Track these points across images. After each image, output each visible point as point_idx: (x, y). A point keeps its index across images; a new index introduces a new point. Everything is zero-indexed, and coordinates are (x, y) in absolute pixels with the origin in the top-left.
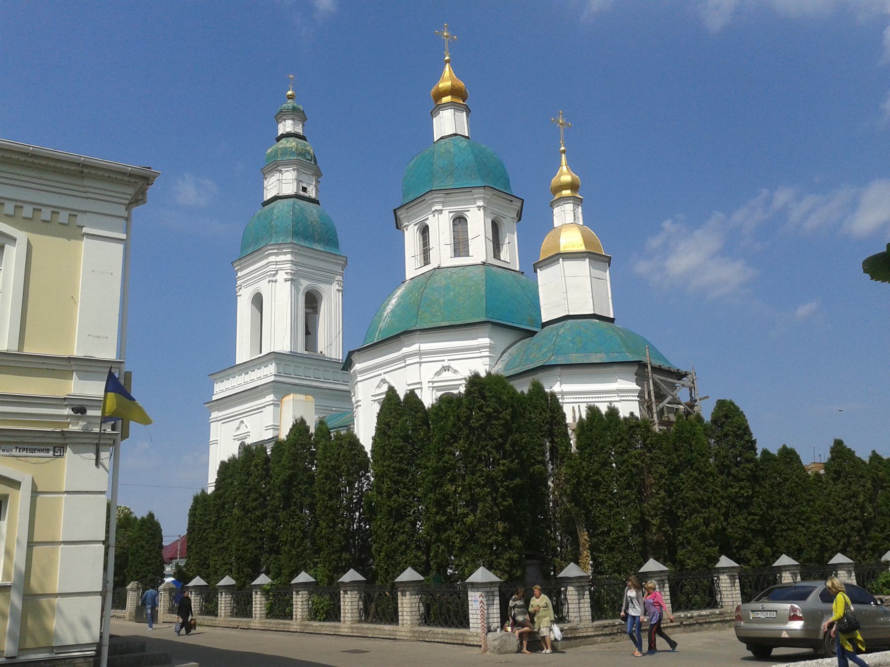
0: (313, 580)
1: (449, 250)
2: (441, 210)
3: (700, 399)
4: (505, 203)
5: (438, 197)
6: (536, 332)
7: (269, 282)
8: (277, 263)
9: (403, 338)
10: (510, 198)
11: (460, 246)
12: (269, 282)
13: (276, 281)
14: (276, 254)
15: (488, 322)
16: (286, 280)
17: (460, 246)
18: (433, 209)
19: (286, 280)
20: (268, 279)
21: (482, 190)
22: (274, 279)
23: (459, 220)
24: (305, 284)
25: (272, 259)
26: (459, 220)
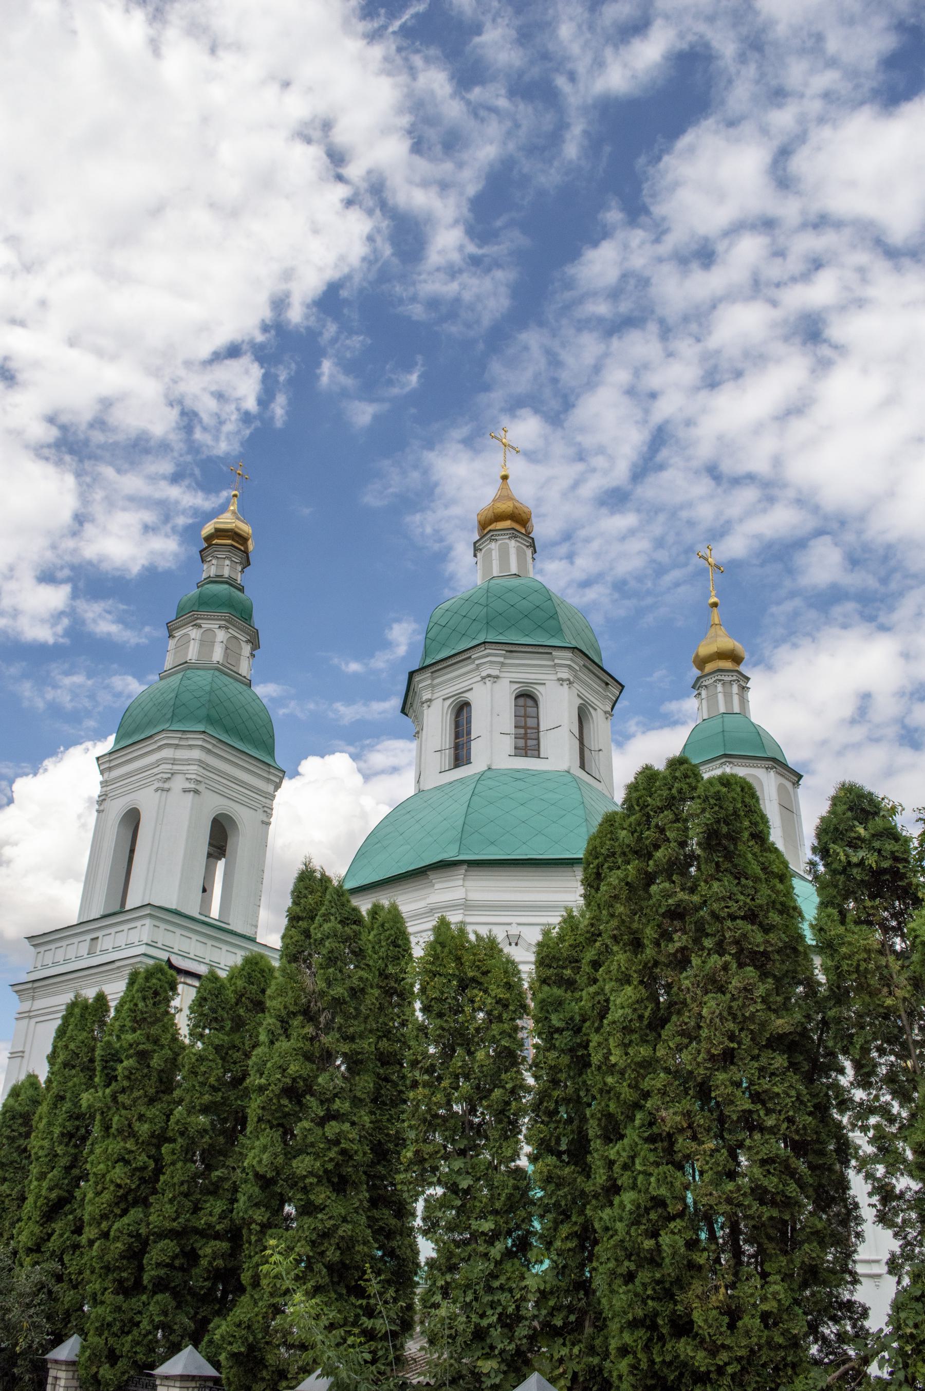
0: (211, 1371)
1: (508, 744)
2: (497, 677)
3: (877, 1261)
4: (597, 685)
5: (496, 656)
7: (157, 790)
8: (174, 761)
9: (432, 875)
10: (609, 680)
11: (528, 740)
12: (157, 790)
13: (168, 790)
14: (177, 746)
15: (725, 756)
16: (185, 791)
17: (528, 740)
18: (484, 674)
19: (185, 791)
20: (155, 787)
21: (569, 654)
22: (166, 786)
23: (526, 698)
24: (213, 804)
25: (167, 753)
26: (526, 698)
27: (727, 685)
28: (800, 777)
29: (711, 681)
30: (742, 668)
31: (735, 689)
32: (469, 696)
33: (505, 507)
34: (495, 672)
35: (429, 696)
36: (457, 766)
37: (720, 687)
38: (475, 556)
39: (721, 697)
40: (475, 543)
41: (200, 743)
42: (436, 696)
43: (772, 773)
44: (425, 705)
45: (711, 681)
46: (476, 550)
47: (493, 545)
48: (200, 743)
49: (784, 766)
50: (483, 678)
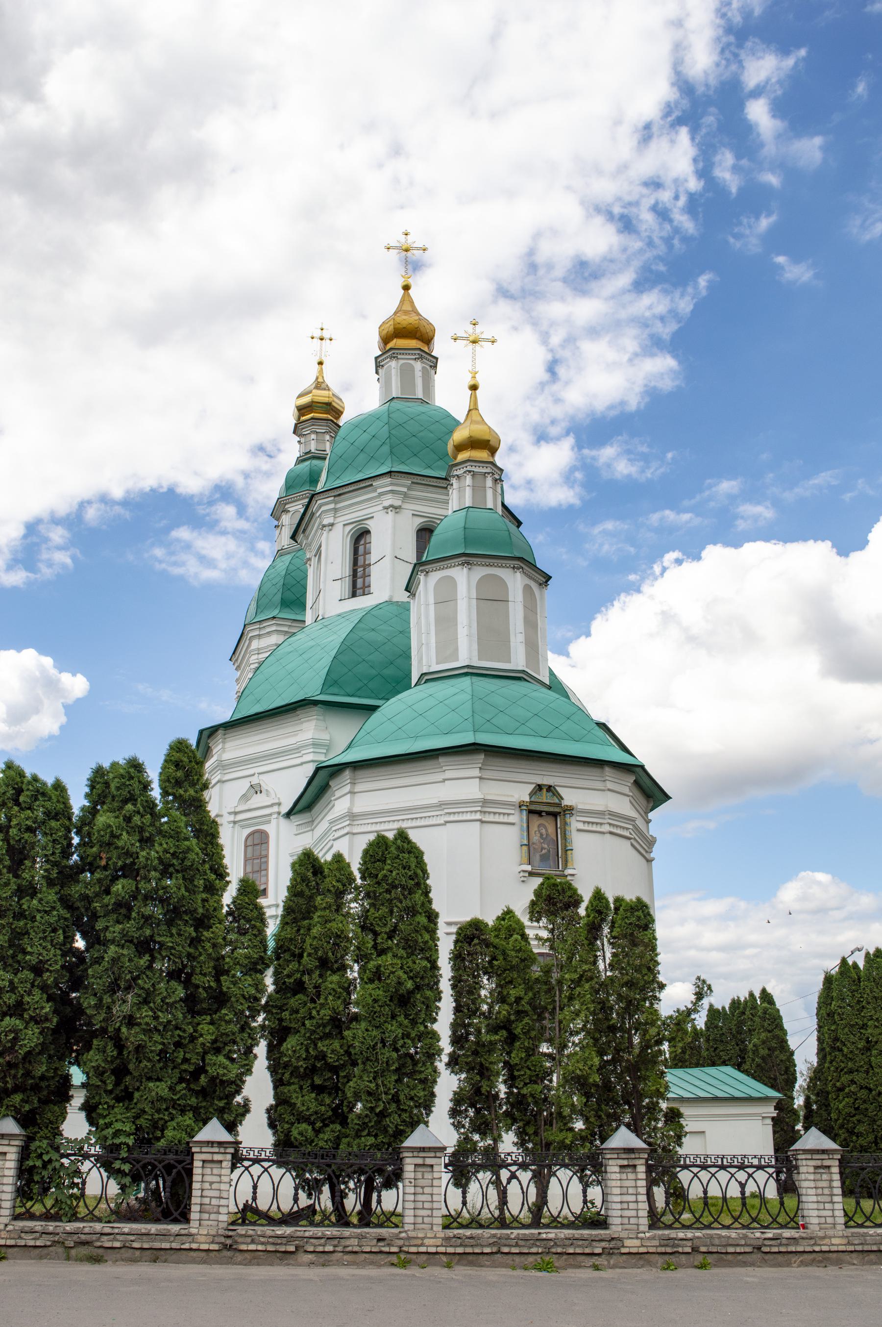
1: (341, 588)
2: (399, 507)
6: (378, 707)
27: (478, 477)
28: (549, 578)
29: (462, 471)
30: (499, 459)
31: (489, 482)
32: (371, 525)
33: (406, 320)
34: (397, 503)
35: (331, 520)
36: (354, 595)
37: (468, 480)
38: (377, 373)
39: (489, 493)
40: (376, 358)
41: (274, 628)
42: (338, 520)
43: (518, 575)
44: (327, 529)
45: (462, 471)
46: (378, 366)
47: (393, 363)
48: (274, 628)
49: (533, 566)
50: (386, 508)
